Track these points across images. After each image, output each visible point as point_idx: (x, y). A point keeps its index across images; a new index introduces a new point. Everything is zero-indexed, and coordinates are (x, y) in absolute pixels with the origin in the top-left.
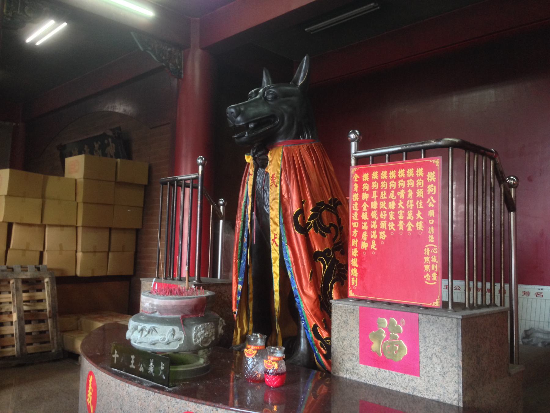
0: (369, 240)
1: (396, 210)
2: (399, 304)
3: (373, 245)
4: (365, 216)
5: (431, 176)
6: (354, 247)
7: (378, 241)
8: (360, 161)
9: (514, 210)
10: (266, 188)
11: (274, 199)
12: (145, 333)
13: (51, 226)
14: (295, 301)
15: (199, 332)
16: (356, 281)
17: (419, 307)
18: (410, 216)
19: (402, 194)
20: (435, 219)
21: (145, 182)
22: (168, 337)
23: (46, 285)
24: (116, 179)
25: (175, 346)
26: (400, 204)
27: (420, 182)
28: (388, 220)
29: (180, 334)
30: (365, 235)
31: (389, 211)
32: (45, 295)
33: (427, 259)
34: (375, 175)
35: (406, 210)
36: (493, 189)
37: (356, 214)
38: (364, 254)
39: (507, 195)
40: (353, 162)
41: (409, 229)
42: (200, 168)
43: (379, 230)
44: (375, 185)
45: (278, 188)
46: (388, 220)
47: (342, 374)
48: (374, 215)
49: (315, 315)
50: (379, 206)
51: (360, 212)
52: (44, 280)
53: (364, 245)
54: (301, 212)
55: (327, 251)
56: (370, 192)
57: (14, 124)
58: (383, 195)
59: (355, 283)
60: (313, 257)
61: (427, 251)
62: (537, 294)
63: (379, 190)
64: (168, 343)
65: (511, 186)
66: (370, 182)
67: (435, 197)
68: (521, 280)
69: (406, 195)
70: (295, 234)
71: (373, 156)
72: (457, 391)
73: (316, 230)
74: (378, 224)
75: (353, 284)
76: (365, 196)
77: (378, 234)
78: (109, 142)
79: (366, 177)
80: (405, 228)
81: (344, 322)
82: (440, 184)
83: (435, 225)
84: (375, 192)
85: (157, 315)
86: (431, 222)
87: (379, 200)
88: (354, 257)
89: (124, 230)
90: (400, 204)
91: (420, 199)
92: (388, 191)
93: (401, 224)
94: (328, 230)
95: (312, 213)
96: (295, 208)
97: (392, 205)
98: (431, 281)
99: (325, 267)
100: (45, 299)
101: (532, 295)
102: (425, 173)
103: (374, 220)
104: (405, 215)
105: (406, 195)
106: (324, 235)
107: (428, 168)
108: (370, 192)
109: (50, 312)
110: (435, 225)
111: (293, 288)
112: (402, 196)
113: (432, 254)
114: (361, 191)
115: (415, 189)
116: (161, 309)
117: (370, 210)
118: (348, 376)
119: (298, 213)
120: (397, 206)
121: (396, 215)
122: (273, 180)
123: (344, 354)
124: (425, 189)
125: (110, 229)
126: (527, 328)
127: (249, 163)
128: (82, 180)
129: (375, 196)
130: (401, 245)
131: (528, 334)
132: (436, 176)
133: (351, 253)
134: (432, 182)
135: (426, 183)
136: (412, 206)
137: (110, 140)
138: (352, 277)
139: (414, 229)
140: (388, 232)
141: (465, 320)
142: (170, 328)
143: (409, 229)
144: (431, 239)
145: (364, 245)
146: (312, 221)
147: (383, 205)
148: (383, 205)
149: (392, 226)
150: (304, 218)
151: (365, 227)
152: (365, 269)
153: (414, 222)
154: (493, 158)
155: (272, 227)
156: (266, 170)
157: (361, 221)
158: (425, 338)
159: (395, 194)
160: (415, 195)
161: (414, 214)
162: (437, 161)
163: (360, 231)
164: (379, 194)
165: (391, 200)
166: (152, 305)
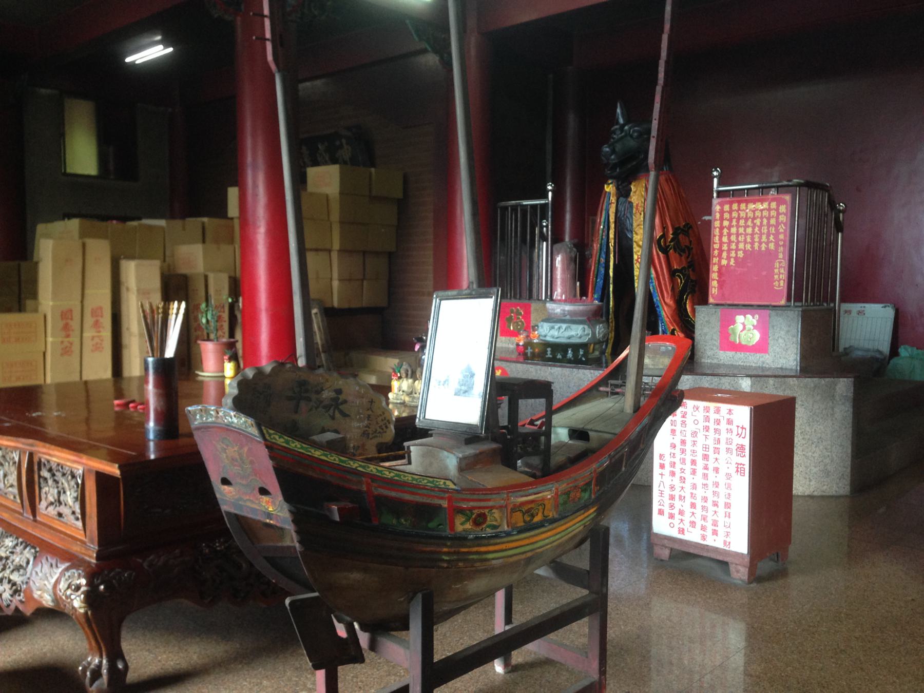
0: (729, 258)
1: (752, 235)
2: (752, 306)
3: (732, 262)
4: (725, 239)
5: (783, 209)
7: (736, 258)
8: (719, 193)
9: (842, 232)
10: (629, 215)
12: (562, 330)
14: (656, 311)
15: (600, 330)
17: (768, 306)
18: (764, 238)
19: (758, 222)
20: (784, 241)
21: (401, 196)
22: (580, 332)
23: (313, 316)
24: (370, 191)
25: (585, 340)
26: (756, 229)
27: (773, 213)
28: (745, 242)
29: (588, 331)
30: (725, 255)
31: (746, 235)
33: (776, 271)
34: (735, 206)
35: (761, 234)
36: (826, 215)
38: (724, 269)
39: (837, 219)
40: (715, 195)
41: (763, 249)
42: (550, 194)
43: (737, 250)
44: (735, 214)
46: (745, 242)
47: (703, 360)
48: (733, 238)
49: (675, 321)
50: (738, 231)
51: (721, 236)
53: (724, 262)
55: (683, 268)
56: (731, 220)
57: (170, 110)
58: (742, 222)
60: (672, 273)
61: (777, 265)
62: (859, 313)
63: (738, 219)
64: (580, 337)
65: (840, 211)
66: (730, 212)
67: (785, 224)
68: (844, 300)
69: (761, 223)
71: (733, 190)
72: (796, 360)
74: (737, 245)
76: (726, 223)
77: (736, 253)
78: (342, 144)
79: (727, 208)
80: (760, 247)
82: (789, 214)
83: (784, 246)
84: (734, 221)
85: (568, 317)
86: (781, 243)
87: (738, 226)
89: (377, 254)
90: (756, 229)
91: (772, 226)
92: (746, 219)
93: (756, 245)
94: (683, 251)
96: (658, 233)
97: (749, 230)
98: (779, 286)
101: (854, 313)
102: (778, 206)
104: (760, 238)
105: (761, 223)
106: (681, 255)
107: (780, 202)
108: (731, 220)
109: (323, 346)
110: (784, 246)
112: (758, 223)
113: (780, 267)
114: (722, 219)
115: (769, 219)
116: (571, 313)
117: (729, 235)
120: (753, 231)
121: (753, 239)
122: (637, 209)
124: (777, 218)
125: (364, 253)
126: (847, 346)
127: (610, 193)
128: (338, 195)
129: (734, 223)
130: (757, 260)
131: (847, 351)
132: (787, 208)
134: (783, 213)
135: (778, 214)
136: (766, 231)
137: (344, 141)
139: (767, 249)
140: (745, 251)
141: (802, 311)
142: (581, 327)
143: (763, 249)
144: (781, 256)
145: (724, 262)
147: (741, 230)
148: (741, 230)
149: (748, 247)
151: (725, 247)
152: (724, 281)
153: (767, 243)
154: (828, 191)
155: (636, 249)
157: (721, 243)
158: (773, 327)
159: (753, 222)
160: (768, 222)
161: (768, 237)
162: (788, 198)
163: (721, 251)
164: (738, 221)
165: (748, 226)
166: (564, 310)
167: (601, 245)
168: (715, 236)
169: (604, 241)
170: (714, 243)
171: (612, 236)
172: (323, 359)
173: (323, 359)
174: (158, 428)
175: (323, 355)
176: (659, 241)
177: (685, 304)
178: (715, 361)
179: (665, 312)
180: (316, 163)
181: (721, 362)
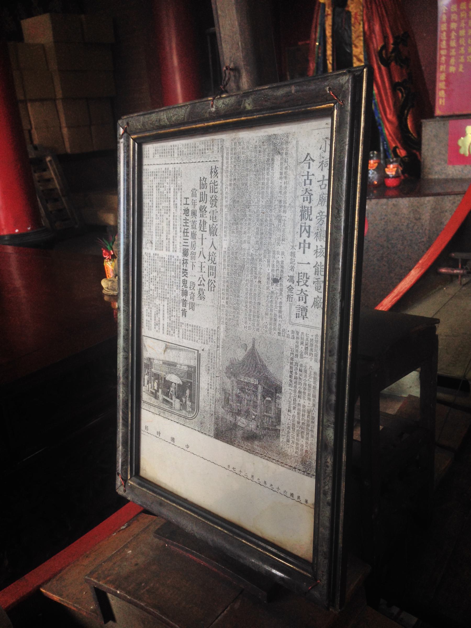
3: (461, 67)
4: (453, 44)
6: (442, 72)
11: (358, 37)
13: (32, 101)
16: (444, 101)
32: (51, 174)
37: (444, 43)
45: (362, 26)
47: (430, 177)
49: (397, 138)
52: (45, 159)
54: (385, 47)
59: (442, 103)
60: (395, 87)
70: (379, 68)
73: (396, 63)
75: (440, 103)
77: (465, 58)
81: (434, 136)
88: (441, 81)
95: (392, 46)
99: (402, 96)
100: (53, 178)
103: (462, 46)
106: (401, 67)
111: (377, 118)
118: (436, 177)
119: (382, 48)
122: (356, 18)
123: (433, 161)
133: (439, 77)
138: (439, 98)
145: (452, 69)
146: (393, 55)
150: (387, 51)
156: (347, 9)
157: (449, 48)
167: (317, 64)
168: (441, 41)
169: (321, 60)
170: (441, 49)
171: (329, 52)
172: (64, 202)
173: (64, 202)
174: (124, 450)
175: (63, 199)
176: (380, 53)
177: (406, 119)
178: (443, 176)
179: (388, 130)
180: (30, 15)
181: (450, 177)
